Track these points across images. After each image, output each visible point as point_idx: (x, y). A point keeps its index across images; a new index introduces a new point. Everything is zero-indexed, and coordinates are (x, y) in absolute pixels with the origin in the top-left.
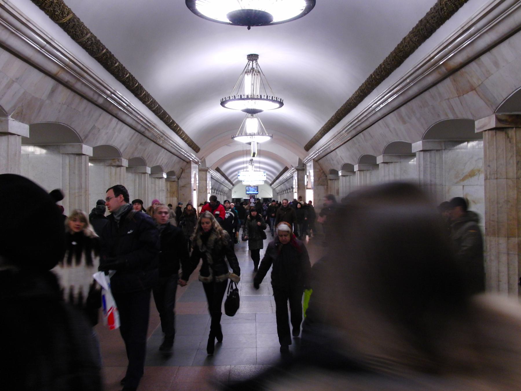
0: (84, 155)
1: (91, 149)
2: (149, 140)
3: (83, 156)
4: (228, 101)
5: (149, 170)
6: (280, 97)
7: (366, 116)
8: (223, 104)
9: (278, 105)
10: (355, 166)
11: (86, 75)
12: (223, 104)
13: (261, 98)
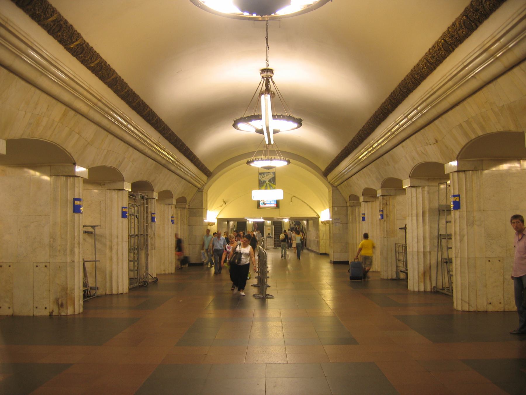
0: (77, 177)
5: (155, 195)
8: (235, 125)
10: (377, 192)
11: (181, 166)
12: (235, 125)
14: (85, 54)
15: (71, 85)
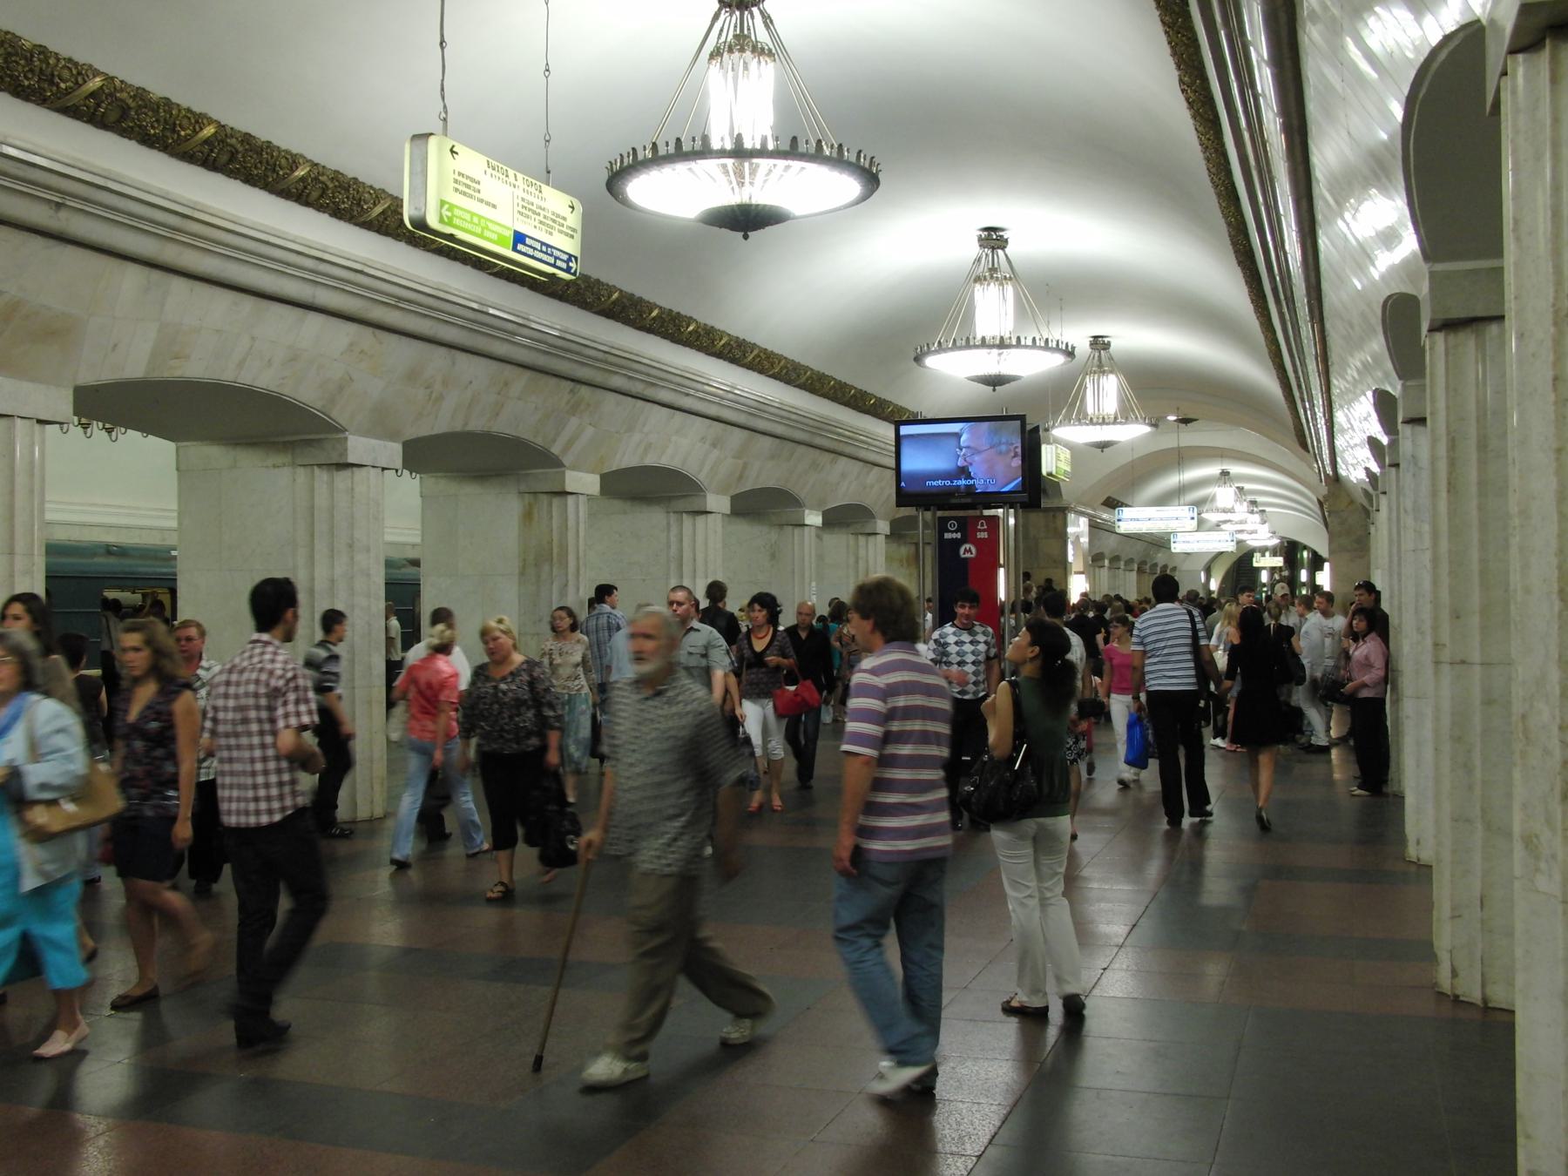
1: (597, 478)
3: (570, 499)
14: (737, 352)
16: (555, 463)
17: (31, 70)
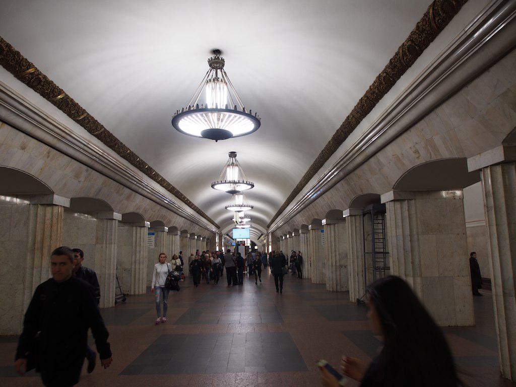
1: (121, 215)
2: (162, 207)
3: (114, 221)
4: (217, 184)
6: (251, 181)
7: (348, 159)
8: (213, 186)
9: (250, 187)
12: (213, 186)
13: (239, 183)
14: (162, 182)
15: (84, 148)
16: (113, 211)
17: (14, 59)
